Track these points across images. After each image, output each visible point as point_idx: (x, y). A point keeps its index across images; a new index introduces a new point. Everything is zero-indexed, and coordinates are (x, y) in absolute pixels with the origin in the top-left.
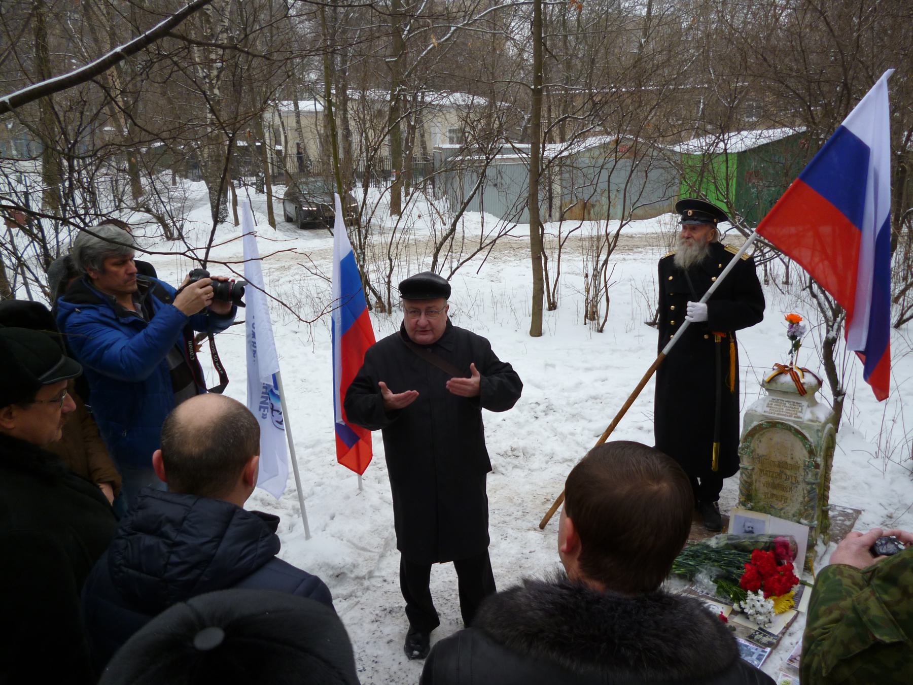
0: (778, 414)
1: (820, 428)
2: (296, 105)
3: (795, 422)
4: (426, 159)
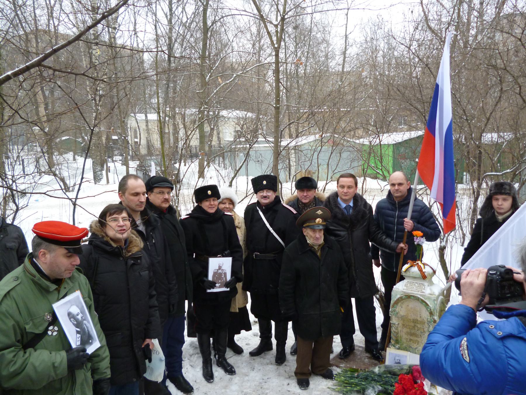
0: (411, 291)
1: (435, 299)
2: (146, 116)
3: (421, 295)
4: (220, 147)
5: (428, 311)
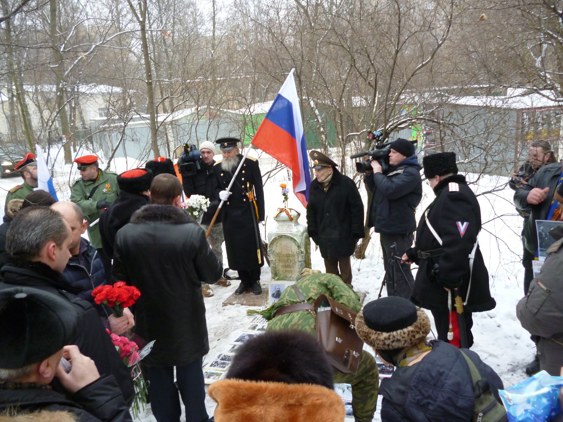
3: (290, 234)
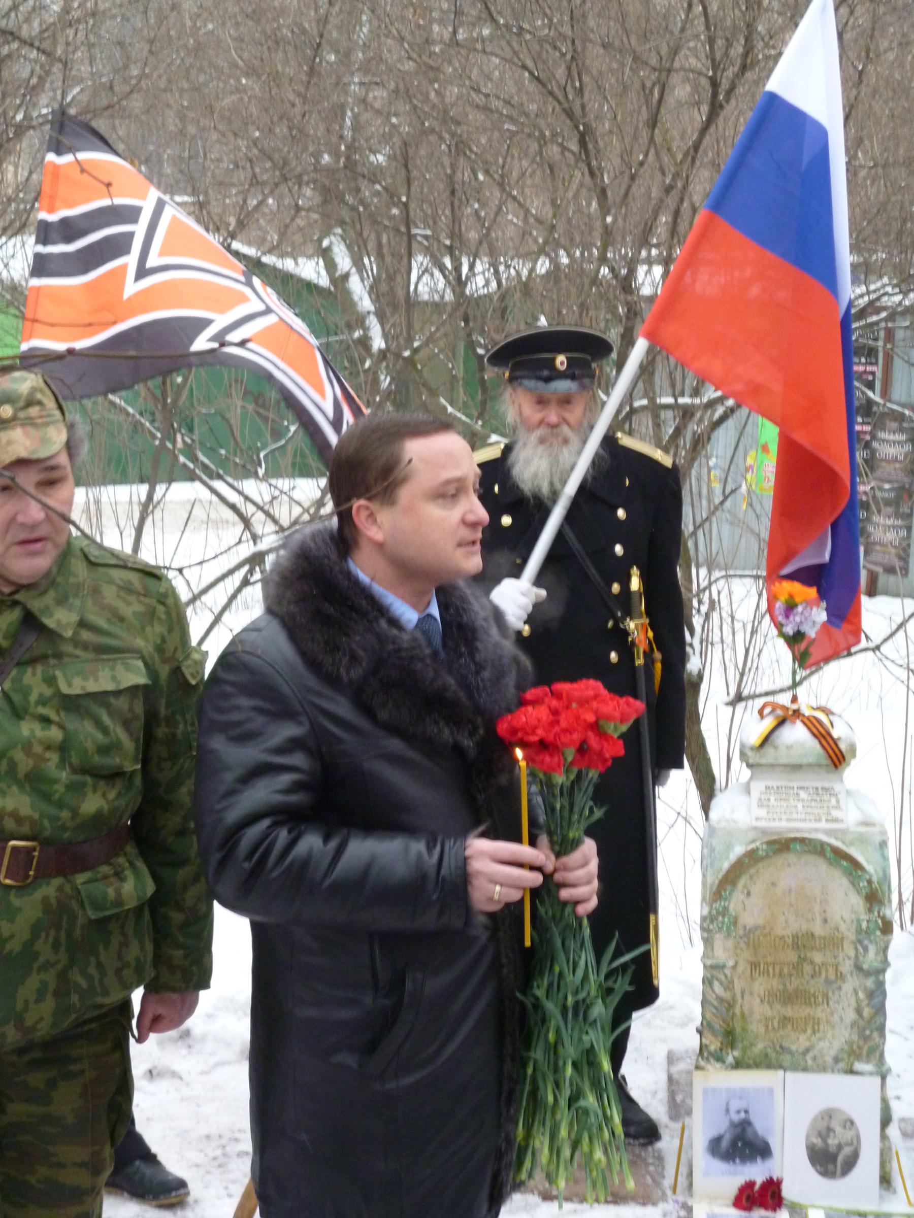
0: (789, 820)
3: (829, 832)
5: (858, 891)
